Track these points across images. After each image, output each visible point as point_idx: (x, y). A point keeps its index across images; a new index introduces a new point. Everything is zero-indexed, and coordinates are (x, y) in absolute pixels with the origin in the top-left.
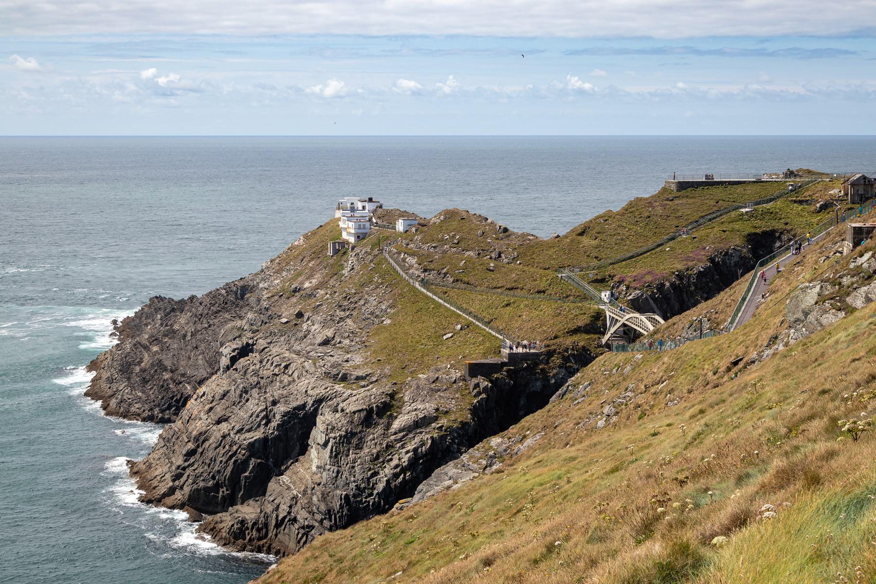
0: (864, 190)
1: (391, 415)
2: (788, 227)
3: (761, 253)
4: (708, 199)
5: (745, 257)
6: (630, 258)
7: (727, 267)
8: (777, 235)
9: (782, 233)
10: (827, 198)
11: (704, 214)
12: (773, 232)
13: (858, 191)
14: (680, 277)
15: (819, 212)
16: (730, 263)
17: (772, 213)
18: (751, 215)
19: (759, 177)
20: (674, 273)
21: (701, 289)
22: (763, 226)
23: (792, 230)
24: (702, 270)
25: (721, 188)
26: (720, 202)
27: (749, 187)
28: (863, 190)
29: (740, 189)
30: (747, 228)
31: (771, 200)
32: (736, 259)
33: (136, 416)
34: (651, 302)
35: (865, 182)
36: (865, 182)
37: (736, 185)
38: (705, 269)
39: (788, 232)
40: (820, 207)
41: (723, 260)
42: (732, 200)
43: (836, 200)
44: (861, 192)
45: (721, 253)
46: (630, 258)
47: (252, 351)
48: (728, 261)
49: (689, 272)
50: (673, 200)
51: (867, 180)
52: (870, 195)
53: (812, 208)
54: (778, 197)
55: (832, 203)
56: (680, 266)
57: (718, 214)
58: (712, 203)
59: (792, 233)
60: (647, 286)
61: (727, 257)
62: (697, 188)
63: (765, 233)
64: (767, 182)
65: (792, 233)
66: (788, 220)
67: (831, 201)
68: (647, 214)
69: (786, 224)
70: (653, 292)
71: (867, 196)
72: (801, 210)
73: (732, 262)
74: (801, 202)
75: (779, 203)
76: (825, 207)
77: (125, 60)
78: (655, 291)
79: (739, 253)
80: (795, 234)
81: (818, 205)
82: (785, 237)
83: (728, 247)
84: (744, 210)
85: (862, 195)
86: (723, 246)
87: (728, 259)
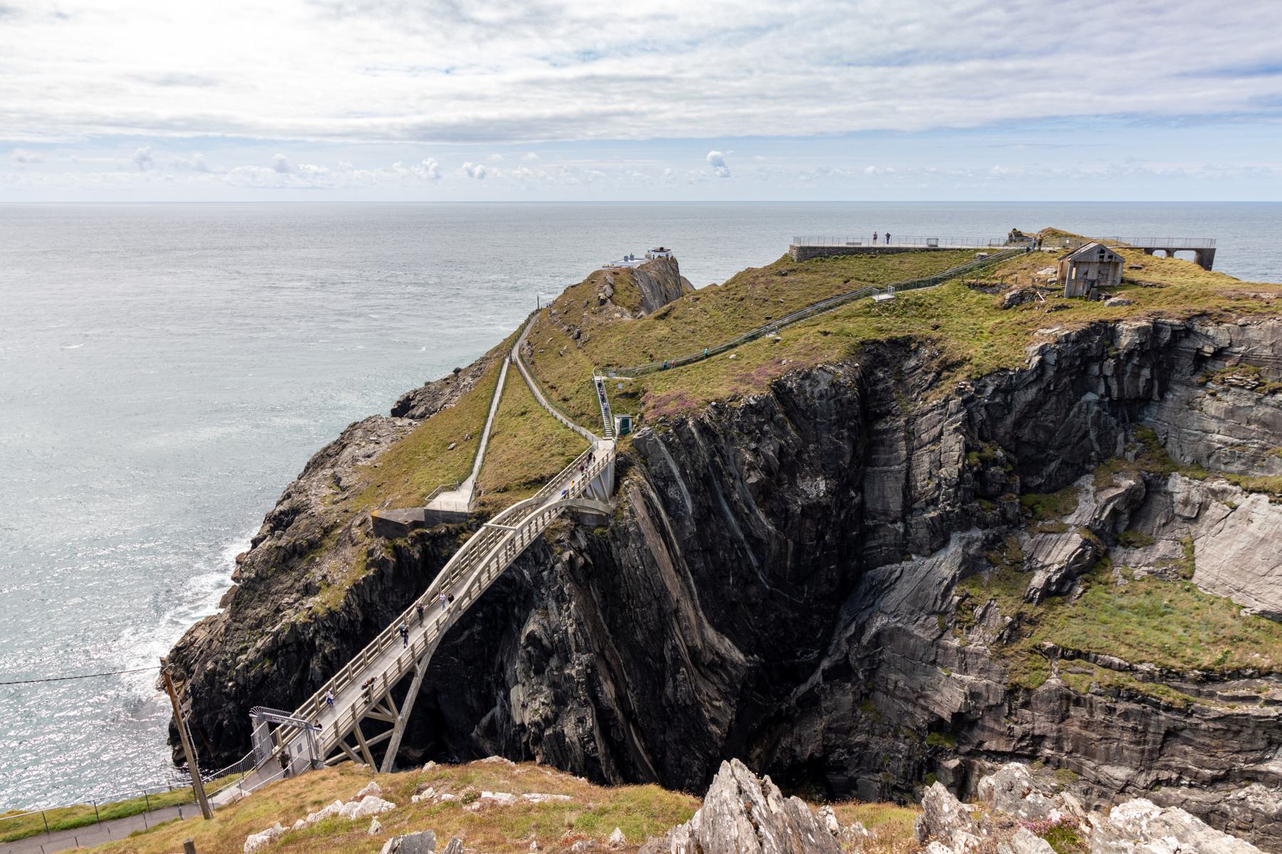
0: (1099, 272)
1: (313, 559)
2: (936, 334)
3: (881, 375)
4: (830, 278)
5: (840, 386)
6: (684, 364)
7: (806, 399)
8: (913, 346)
9: (921, 343)
10: (1028, 283)
11: (816, 300)
12: (909, 339)
13: (1086, 273)
14: (720, 408)
15: (1006, 308)
16: (813, 393)
17: (921, 305)
18: (885, 307)
19: (933, 242)
20: (709, 403)
21: (749, 433)
22: (896, 327)
23: (939, 340)
24: (753, 402)
25: (865, 258)
26: (852, 281)
27: (912, 258)
28: (1096, 273)
29: (894, 260)
30: (865, 329)
31: (935, 282)
32: (823, 386)
33: (1106, 488)
34: (663, 448)
35: (1102, 257)
36: (1102, 257)
37: (892, 253)
38: (759, 402)
39: (934, 342)
40: (1010, 300)
41: (800, 386)
42: (871, 279)
43: (1041, 288)
44: (1093, 275)
45: (799, 373)
46: (684, 364)
47: (1178, 736)
48: (808, 389)
49: (734, 404)
50: (786, 275)
51: (1106, 255)
52: (1109, 283)
53: (997, 300)
54: (951, 277)
55: (1034, 294)
56: (723, 392)
57: (839, 300)
58: (839, 281)
59: (939, 345)
60: (661, 422)
61: (807, 383)
62: (828, 257)
63: (893, 342)
64: (944, 250)
65: (939, 345)
66: (942, 321)
67: (1032, 290)
68: (742, 294)
69: (936, 327)
70: (667, 433)
71: (1103, 284)
72: (976, 303)
73: (816, 390)
74: (982, 288)
75: (945, 288)
76: (1019, 300)
77: (430, 589)
78: (671, 431)
79: (830, 377)
80: (944, 348)
81: (1008, 296)
82: (925, 352)
83: (812, 363)
84: (877, 298)
85: (1093, 282)
86: (806, 362)
87: (810, 385)
